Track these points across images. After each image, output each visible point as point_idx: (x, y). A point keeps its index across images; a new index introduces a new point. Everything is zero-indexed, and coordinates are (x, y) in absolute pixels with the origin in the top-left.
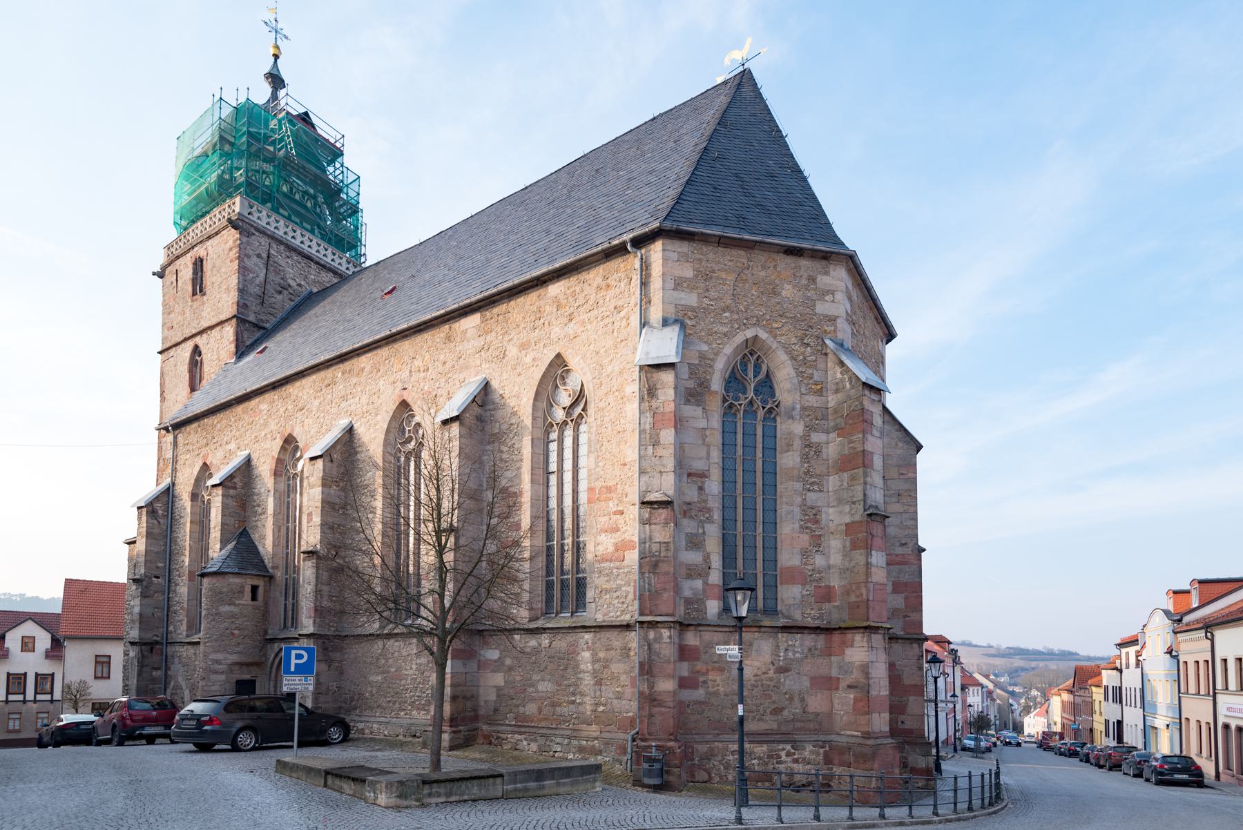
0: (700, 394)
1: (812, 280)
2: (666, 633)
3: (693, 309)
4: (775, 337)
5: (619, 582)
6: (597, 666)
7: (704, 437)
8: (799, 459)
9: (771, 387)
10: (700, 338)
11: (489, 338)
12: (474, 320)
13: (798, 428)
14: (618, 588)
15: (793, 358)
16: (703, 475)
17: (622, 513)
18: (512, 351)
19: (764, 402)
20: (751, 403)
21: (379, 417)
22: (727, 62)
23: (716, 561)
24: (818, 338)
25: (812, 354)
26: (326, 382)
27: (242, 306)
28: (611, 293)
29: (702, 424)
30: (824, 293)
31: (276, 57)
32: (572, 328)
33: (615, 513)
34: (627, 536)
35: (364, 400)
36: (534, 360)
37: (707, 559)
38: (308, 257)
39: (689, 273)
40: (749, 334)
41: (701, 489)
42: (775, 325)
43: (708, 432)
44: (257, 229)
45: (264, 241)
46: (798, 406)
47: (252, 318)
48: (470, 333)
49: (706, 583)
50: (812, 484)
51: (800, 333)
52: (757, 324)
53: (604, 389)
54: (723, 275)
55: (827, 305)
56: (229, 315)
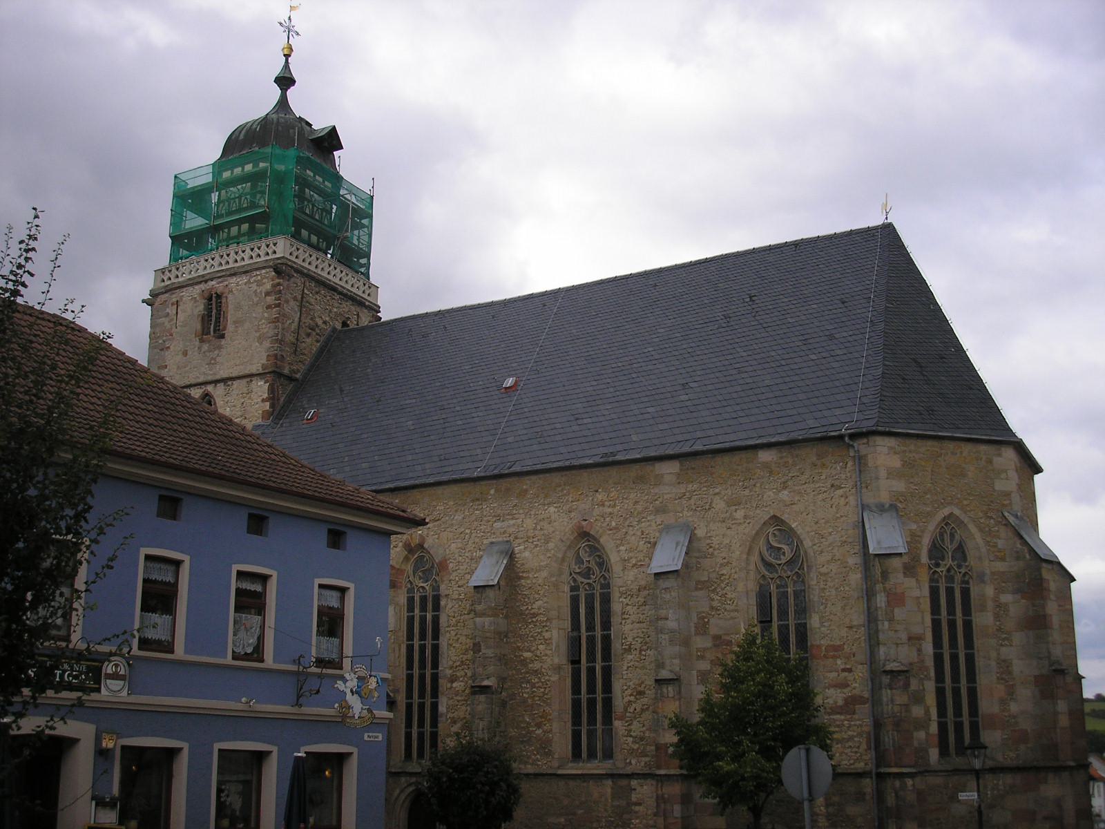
0: (914, 567)
1: (990, 462)
2: (909, 782)
4: (965, 513)
5: (850, 733)
6: (831, 810)
7: (919, 604)
8: (992, 618)
9: (963, 552)
12: (671, 468)
13: (990, 591)
14: (851, 738)
15: (981, 530)
17: (850, 670)
18: (719, 504)
19: (959, 566)
20: (949, 570)
21: (551, 545)
23: (934, 712)
24: (998, 511)
27: (277, 358)
29: (917, 593)
31: (287, 56)
32: (785, 495)
33: (843, 670)
34: (857, 692)
35: (529, 523)
36: (745, 517)
37: (927, 712)
38: (333, 289)
40: (946, 511)
41: (919, 650)
42: (965, 502)
44: (297, 271)
45: (299, 280)
47: (286, 371)
49: (927, 734)
50: (1004, 639)
51: (985, 508)
52: (949, 504)
56: (255, 368)
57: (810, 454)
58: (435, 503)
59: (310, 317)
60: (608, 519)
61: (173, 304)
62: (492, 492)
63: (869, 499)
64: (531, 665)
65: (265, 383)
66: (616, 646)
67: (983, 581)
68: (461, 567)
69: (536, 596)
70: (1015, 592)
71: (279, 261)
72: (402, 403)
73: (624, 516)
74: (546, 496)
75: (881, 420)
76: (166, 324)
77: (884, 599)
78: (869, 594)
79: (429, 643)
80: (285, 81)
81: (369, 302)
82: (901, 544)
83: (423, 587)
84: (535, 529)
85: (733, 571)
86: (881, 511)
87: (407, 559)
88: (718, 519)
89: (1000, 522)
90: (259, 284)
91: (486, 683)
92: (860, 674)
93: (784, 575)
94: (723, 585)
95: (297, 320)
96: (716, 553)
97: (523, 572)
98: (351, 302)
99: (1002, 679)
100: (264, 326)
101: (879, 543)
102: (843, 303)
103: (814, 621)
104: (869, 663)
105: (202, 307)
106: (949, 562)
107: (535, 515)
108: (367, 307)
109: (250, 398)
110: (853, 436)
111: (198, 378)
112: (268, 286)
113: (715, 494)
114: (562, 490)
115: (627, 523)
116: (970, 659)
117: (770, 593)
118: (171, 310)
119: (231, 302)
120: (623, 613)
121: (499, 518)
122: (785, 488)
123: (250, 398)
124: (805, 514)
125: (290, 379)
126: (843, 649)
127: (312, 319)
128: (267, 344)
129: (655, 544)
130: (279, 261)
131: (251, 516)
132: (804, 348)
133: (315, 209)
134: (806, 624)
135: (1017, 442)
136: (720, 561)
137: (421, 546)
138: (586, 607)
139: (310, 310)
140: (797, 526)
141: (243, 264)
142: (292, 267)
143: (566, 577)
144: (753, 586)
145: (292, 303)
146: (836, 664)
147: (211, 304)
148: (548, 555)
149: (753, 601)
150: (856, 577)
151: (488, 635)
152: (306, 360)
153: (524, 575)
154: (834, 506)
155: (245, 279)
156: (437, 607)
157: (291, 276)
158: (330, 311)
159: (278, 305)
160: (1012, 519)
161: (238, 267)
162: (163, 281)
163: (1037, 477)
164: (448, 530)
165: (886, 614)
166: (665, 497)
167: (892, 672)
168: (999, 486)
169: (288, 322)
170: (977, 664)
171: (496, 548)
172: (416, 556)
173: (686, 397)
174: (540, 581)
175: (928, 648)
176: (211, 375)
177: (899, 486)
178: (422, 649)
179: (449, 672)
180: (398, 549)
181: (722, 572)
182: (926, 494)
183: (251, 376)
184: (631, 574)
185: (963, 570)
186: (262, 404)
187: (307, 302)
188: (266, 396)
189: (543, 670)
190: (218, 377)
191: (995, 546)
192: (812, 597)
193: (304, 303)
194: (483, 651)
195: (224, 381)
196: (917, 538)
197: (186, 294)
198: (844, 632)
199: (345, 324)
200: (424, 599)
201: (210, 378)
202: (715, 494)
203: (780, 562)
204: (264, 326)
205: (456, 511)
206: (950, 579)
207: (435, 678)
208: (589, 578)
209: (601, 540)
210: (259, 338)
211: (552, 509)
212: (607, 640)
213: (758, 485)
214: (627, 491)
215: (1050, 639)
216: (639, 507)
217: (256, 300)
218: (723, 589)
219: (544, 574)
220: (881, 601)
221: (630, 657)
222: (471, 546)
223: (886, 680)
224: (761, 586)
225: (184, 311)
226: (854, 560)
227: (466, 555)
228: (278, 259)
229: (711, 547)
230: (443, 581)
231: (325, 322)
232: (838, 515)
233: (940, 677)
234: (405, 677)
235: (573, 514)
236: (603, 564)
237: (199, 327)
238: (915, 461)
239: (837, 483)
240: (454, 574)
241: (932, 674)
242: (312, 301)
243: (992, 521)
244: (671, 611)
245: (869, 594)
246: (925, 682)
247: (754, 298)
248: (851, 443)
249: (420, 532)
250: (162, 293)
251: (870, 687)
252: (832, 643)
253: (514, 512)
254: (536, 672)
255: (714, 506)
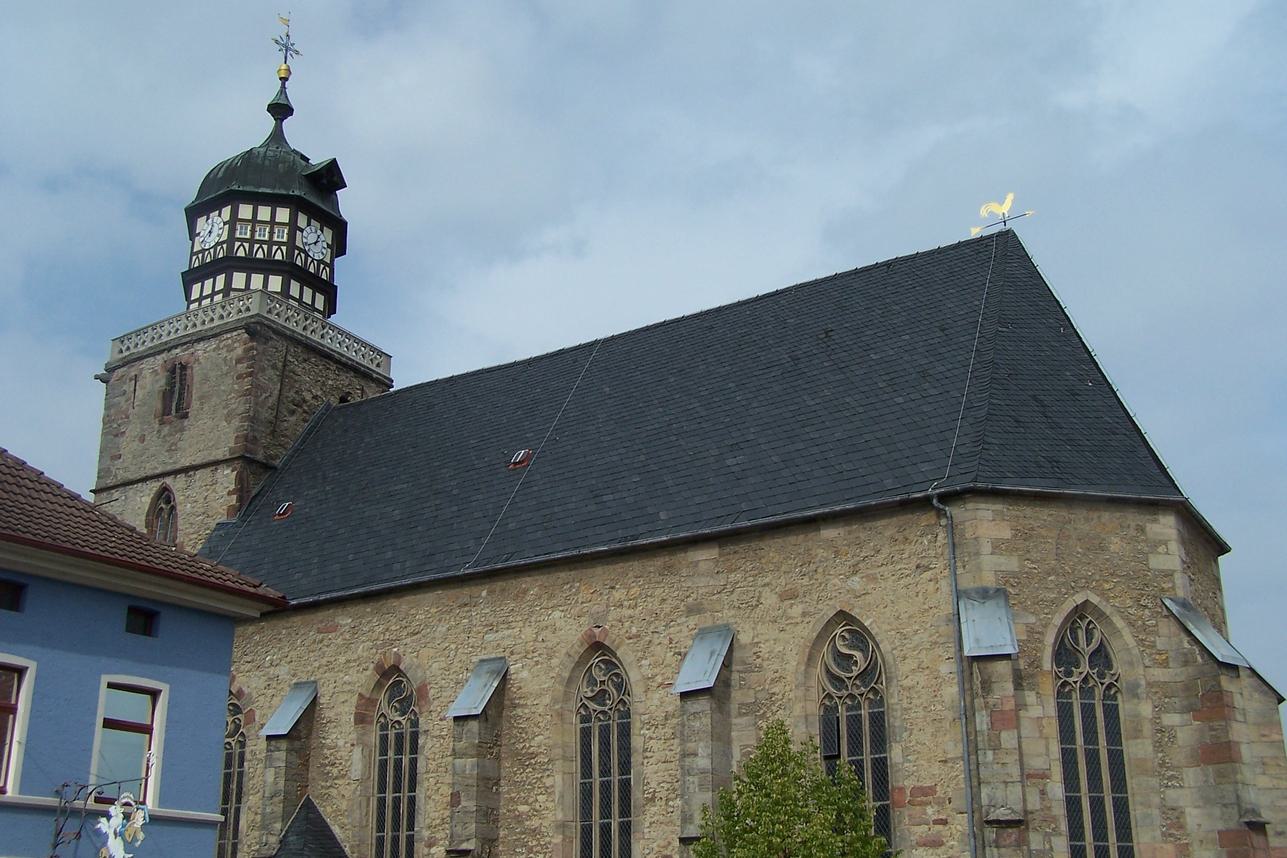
1: (1141, 529)
3: (1014, 575)
8: (1151, 748)
9: (1107, 656)
10: (1025, 609)
11: (732, 577)
12: (705, 556)
13: (1146, 709)
15: (1131, 624)
16: (1044, 776)
17: (944, 822)
18: (770, 599)
19: (1101, 676)
20: (1085, 680)
21: (555, 662)
22: (984, 212)
25: (1152, 617)
26: (460, 601)
27: (249, 439)
28: (909, 549)
30: (1155, 545)
31: (284, 80)
32: (856, 582)
33: (936, 822)
36: (804, 614)
39: (1007, 534)
40: (1079, 599)
41: (1043, 793)
42: (1107, 586)
43: (1044, 722)
44: (276, 332)
45: (281, 345)
46: (1143, 682)
47: (260, 456)
48: (703, 566)
50: (1170, 778)
51: (1135, 593)
53: (911, 664)
54: (1044, 532)
55: (1161, 558)
56: (221, 453)
57: (887, 527)
58: (413, 611)
59: (295, 390)
60: (627, 624)
61: (131, 380)
62: (484, 593)
63: (967, 582)
64: (528, 823)
65: (233, 471)
66: (637, 795)
67: (1136, 696)
68: (444, 694)
69: (536, 729)
70: (1188, 709)
71: (253, 320)
72: (390, 489)
73: (647, 618)
74: (551, 597)
75: (980, 473)
76: (123, 403)
77: (986, 719)
78: (968, 715)
79: (405, 795)
80: (281, 110)
81: (378, 373)
82: (1009, 642)
83: (399, 722)
84: (535, 640)
85: (788, 688)
86: (984, 598)
87: (379, 685)
88: (768, 618)
89: (1158, 612)
90: (230, 349)
91: (464, 846)
92: (959, 827)
93: (856, 692)
94: (774, 708)
95: (276, 392)
96: (765, 664)
97: (520, 698)
98: (352, 374)
99: (1170, 835)
100: (233, 401)
101: (977, 640)
102: (943, 330)
103: (895, 754)
104: (970, 812)
105: (163, 382)
106: (1085, 668)
107: (536, 622)
108: (373, 380)
109: (214, 491)
110: (946, 498)
111: (156, 468)
112: (239, 351)
113: (764, 585)
114: (570, 589)
115: (652, 629)
116: (1122, 808)
117: (838, 718)
118: (129, 387)
119: (196, 373)
120: (645, 750)
121: (492, 628)
122: (855, 573)
123: (214, 491)
124: (882, 606)
125: (266, 467)
126: (936, 792)
127: (297, 392)
128: (236, 423)
129: (685, 654)
130: (253, 320)
131: (133, 611)
132: (889, 389)
133: (310, 260)
134: (886, 758)
135: (1182, 503)
136: (770, 675)
137: (395, 669)
138: (600, 743)
139: (296, 381)
140: (871, 624)
141: (213, 325)
142: (269, 327)
143: (574, 705)
144: (814, 709)
145: (270, 372)
146: (926, 814)
147: (174, 378)
148: (551, 675)
149: (816, 731)
150: (951, 691)
151: (470, 781)
152: (288, 443)
153: (522, 702)
154: (920, 594)
155: (213, 343)
156: (414, 749)
157: (268, 339)
158: (324, 384)
159: (250, 374)
160: (1174, 608)
161: (206, 331)
162: (121, 351)
163: (1221, 559)
164: (429, 645)
165: (990, 740)
166: (700, 592)
167: (998, 822)
168: (1157, 562)
169: (264, 395)
170: (1132, 813)
171: (486, 667)
172: (391, 681)
173: (734, 461)
174: (541, 710)
175: (1057, 789)
176: (171, 464)
177: (1012, 563)
178: (397, 802)
179: (426, 834)
180: (368, 673)
181: (773, 691)
182: (1049, 575)
183: (216, 464)
184: (656, 697)
185: (1107, 681)
186: (228, 498)
187: (290, 372)
188: (232, 487)
189: (543, 829)
190: (178, 466)
191: (1153, 646)
192: (891, 720)
193: (286, 373)
194: (463, 803)
195: (185, 470)
196: (1037, 636)
197: (147, 365)
198: (936, 769)
199: (343, 400)
200: (400, 737)
201: (169, 468)
202: (764, 585)
203: (850, 675)
204: (233, 401)
205: (440, 620)
206: (1087, 692)
207: (411, 841)
208: (605, 705)
209: (618, 654)
210: (228, 415)
211: (557, 614)
212: (626, 786)
213: (820, 570)
214: (652, 586)
215: (1239, 777)
216: (667, 608)
217: (225, 369)
218: (774, 714)
219: (547, 700)
220: (982, 721)
221: (654, 809)
222: (456, 666)
223: (991, 834)
224: (827, 708)
225: (142, 388)
226: (947, 668)
227: (450, 677)
228: (252, 317)
229: (758, 657)
230: (421, 713)
231: (315, 397)
232: (926, 607)
233: (1075, 832)
234: (374, 841)
235: (582, 620)
236: (622, 686)
237: (159, 406)
238: (1032, 529)
239: (924, 562)
240: (436, 703)
241: (1064, 826)
242: (299, 370)
243: (1147, 611)
244: (701, 744)
245: (968, 715)
246: (1052, 838)
247: (830, 334)
248: (941, 507)
249: (395, 650)
250: (120, 367)
251: (972, 843)
252: (920, 784)
253: (511, 619)
254: (535, 832)
255: (762, 600)
